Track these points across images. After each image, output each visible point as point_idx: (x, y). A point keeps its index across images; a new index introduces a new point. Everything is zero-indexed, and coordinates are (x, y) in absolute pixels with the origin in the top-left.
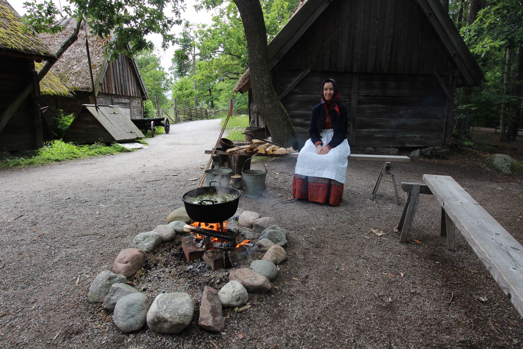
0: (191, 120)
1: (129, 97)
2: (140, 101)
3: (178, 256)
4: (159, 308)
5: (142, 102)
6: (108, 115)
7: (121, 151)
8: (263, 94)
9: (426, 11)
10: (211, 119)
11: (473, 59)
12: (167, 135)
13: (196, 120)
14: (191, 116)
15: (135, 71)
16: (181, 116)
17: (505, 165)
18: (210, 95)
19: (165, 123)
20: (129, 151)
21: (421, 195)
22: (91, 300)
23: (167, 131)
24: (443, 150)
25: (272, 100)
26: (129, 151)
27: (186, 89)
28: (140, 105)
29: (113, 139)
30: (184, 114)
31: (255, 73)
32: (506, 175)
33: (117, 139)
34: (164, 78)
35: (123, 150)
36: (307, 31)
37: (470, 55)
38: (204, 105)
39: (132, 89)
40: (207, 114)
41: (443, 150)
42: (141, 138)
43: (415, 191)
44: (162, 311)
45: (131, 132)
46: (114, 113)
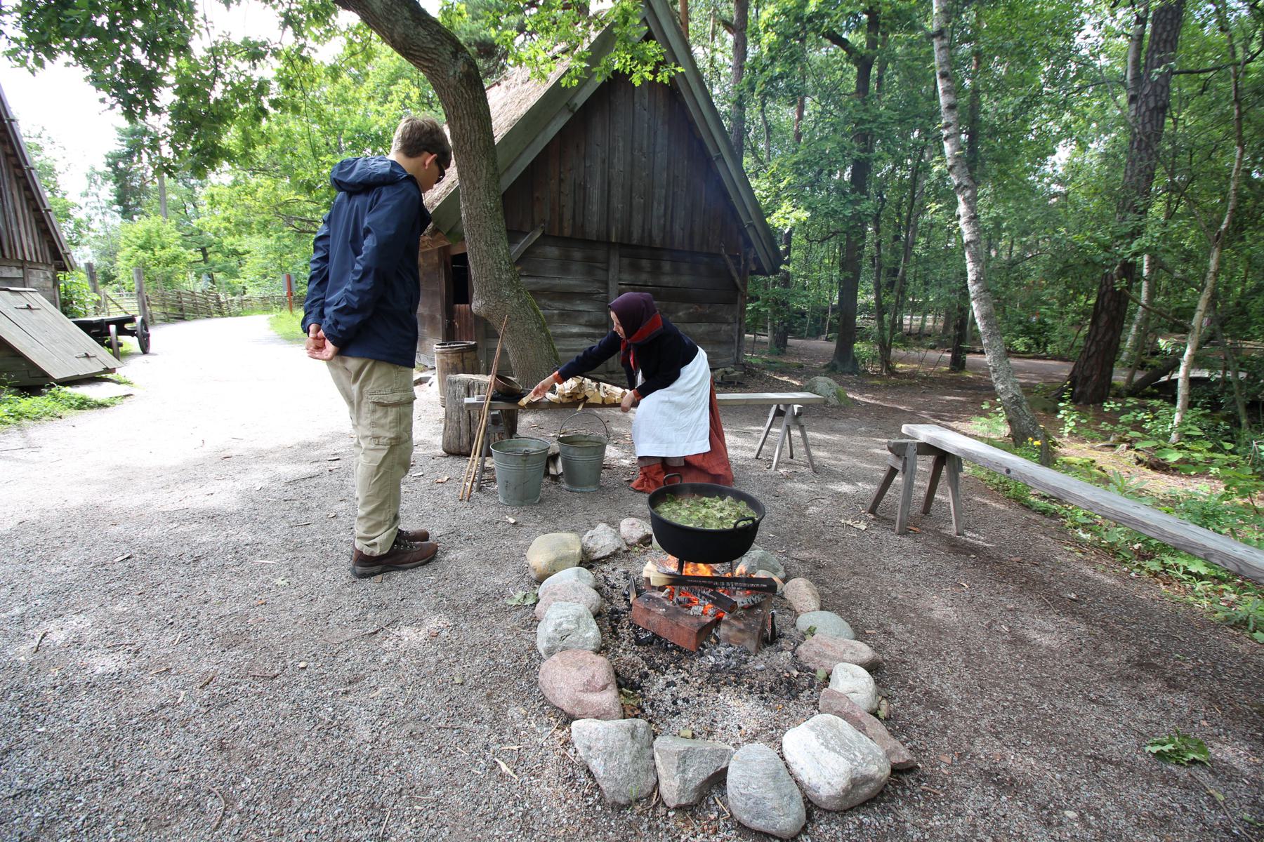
0: (182, 318)
1: (22, 264)
2: (49, 274)
3: (652, 643)
4: (852, 761)
5: (54, 275)
6: (13, 314)
7: (80, 407)
8: (500, 279)
9: (713, 154)
10: (230, 315)
11: (770, 234)
12: (145, 357)
13: (195, 318)
14: (181, 310)
15: (34, 199)
16: (156, 311)
17: (830, 394)
18: (205, 260)
19: (139, 329)
20: (102, 406)
21: (918, 457)
22: (622, 801)
23: (145, 348)
24: (737, 373)
25: (518, 291)
26: (102, 406)
27: (163, 248)
28: (50, 284)
29: (46, 376)
30: (164, 305)
31: (480, 235)
32: (833, 407)
33: (57, 375)
34: (68, 216)
35: (83, 404)
36: (532, 163)
37: (766, 226)
38: (193, 284)
39: (28, 243)
40: (219, 304)
41: (737, 373)
42: (113, 371)
43: (911, 452)
44: (860, 764)
45: (87, 356)
46: (29, 307)
